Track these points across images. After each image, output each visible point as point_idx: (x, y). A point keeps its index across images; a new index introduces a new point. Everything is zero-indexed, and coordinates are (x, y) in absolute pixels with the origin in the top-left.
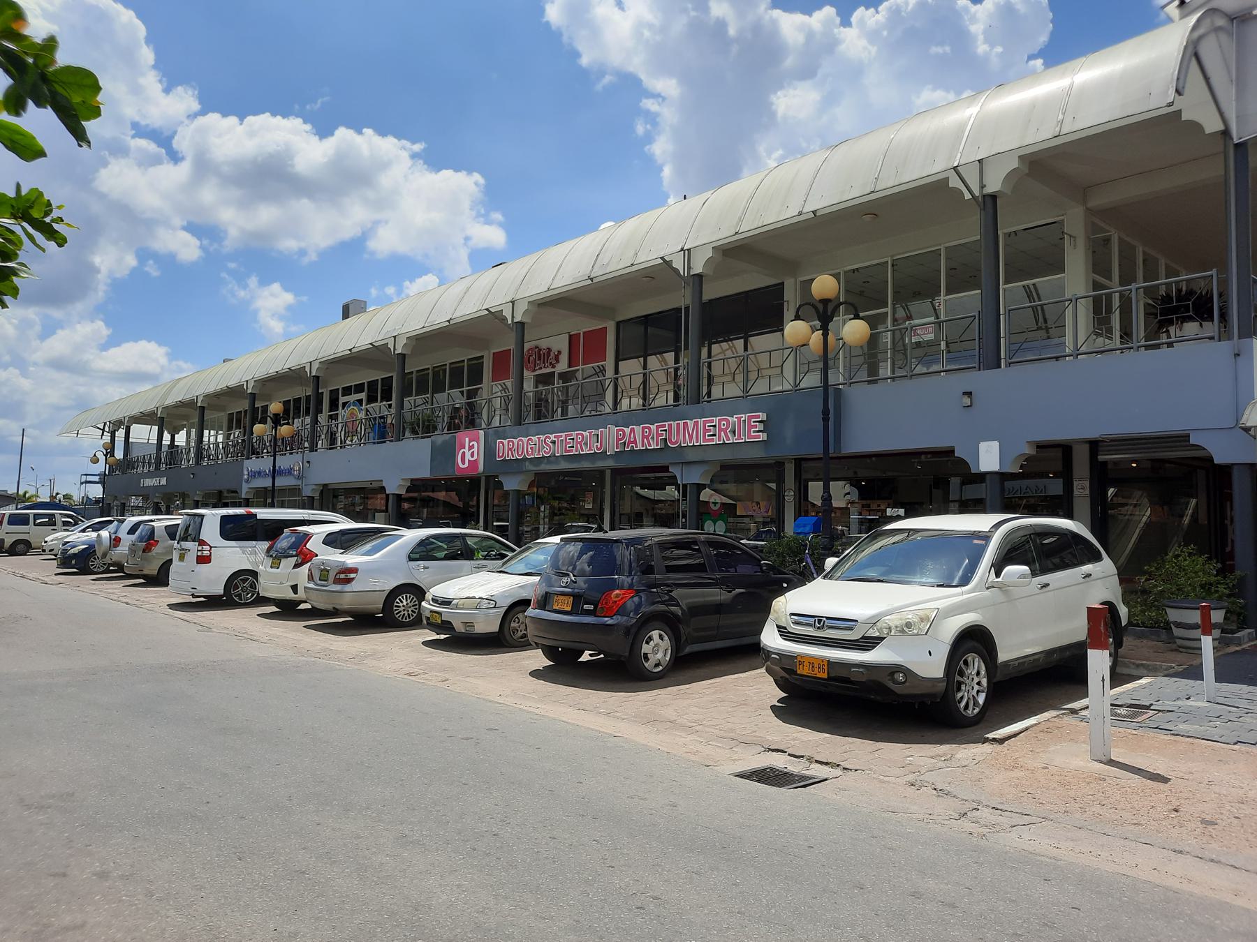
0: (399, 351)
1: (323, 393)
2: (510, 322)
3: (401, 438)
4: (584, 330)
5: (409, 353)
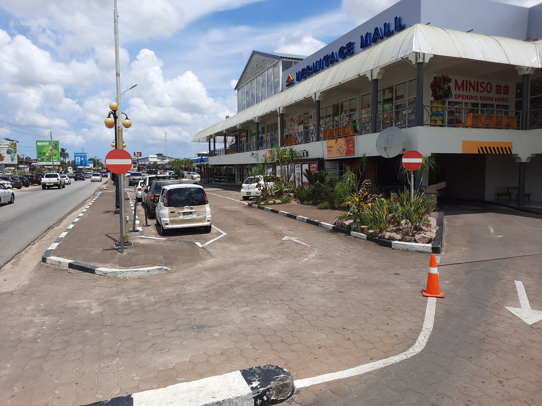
0: (317, 99)
1: (286, 120)
2: (370, 79)
3: (377, 130)
4: (340, 102)
5: (322, 100)
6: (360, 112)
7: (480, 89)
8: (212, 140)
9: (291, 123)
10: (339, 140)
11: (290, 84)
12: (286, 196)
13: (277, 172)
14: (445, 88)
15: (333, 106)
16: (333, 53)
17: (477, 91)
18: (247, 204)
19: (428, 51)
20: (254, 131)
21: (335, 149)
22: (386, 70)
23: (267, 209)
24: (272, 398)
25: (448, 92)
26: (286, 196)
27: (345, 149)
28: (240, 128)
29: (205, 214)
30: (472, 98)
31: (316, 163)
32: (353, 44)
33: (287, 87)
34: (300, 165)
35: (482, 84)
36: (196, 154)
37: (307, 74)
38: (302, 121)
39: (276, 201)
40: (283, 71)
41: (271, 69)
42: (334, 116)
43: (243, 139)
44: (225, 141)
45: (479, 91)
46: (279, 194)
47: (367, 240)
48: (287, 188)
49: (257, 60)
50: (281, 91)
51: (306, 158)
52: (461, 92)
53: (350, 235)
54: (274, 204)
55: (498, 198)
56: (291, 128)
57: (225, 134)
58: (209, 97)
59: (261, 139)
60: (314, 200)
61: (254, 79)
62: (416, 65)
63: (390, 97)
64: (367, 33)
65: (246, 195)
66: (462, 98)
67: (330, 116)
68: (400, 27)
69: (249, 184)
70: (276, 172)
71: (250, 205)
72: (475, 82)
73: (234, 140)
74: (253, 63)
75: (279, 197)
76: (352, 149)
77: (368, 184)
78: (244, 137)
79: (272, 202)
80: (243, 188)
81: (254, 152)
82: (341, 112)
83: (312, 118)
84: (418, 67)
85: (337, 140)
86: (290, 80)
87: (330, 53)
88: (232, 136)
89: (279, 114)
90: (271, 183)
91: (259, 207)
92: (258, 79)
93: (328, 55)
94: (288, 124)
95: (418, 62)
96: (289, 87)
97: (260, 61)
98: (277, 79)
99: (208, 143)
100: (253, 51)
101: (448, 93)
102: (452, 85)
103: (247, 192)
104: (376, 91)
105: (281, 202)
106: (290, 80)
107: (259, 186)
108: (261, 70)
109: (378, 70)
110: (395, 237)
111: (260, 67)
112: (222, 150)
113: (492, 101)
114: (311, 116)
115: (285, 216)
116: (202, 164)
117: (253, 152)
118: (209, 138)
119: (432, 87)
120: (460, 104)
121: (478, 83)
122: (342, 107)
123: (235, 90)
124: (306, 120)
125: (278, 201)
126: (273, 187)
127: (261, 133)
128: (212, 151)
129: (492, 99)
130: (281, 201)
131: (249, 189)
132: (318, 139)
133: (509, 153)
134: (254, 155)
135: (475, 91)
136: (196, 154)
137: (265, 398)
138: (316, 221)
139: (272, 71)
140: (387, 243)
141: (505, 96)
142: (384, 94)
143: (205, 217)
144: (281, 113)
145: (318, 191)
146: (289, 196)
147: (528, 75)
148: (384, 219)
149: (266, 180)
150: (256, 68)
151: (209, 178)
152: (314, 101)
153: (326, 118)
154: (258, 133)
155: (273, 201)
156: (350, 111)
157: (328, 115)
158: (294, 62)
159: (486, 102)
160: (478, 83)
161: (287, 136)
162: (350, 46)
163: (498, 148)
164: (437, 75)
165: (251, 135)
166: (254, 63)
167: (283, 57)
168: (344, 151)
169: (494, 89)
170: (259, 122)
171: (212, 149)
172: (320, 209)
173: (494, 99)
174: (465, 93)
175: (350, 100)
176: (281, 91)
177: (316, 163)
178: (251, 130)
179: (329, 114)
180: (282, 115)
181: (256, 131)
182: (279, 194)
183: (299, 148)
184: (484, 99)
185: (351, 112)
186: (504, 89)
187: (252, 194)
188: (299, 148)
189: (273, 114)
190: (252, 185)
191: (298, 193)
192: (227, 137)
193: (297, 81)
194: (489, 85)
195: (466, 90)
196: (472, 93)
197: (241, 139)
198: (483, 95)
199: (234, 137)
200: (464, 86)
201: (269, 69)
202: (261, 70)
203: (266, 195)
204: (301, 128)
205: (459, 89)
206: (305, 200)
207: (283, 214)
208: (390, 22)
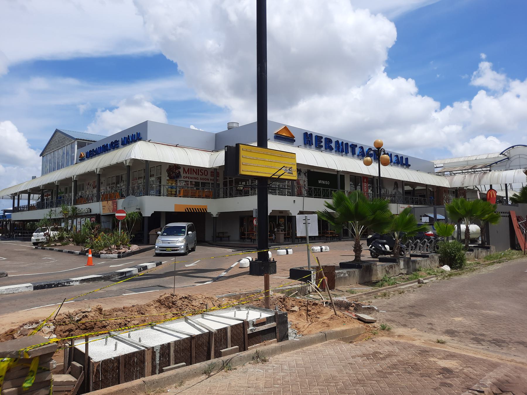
0: (127, 164)
7: (200, 173)
8: (16, 197)
9: (88, 187)
10: (109, 202)
13: (69, 225)
15: (144, 170)
17: (198, 175)
18: (34, 247)
21: (106, 208)
30: (195, 178)
34: (84, 219)
36: (1, 210)
40: (78, 148)
41: (69, 145)
43: (49, 197)
45: (199, 174)
50: (76, 164)
51: (90, 214)
52: (187, 175)
53: (86, 255)
58: (30, 149)
64: (124, 137)
65: (35, 241)
66: (188, 179)
69: (38, 233)
71: (36, 248)
72: (196, 169)
76: (116, 208)
78: (49, 195)
79: (54, 244)
80: (33, 236)
81: (52, 209)
85: (108, 202)
88: (39, 194)
92: (59, 151)
100: (56, 129)
105: (61, 244)
109: (129, 161)
112: (25, 206)
114: (102, 182)
116: (4, 220)
122: (122, 177)
123: (40, 156)
127: (64, 193)
128: (16, 207)
131: (38, 236)
132: (98, 201)
133: (205, 212)
136: (1, 210)
144: (74, 179)
151: (10, 233)
158: (88, 143)
159: (204, 181)
163: (203, 209)
166: (56, 138)
170: (131, 165)
171: (16, 205)
173: (210, 180)
174: (190, 175)
176: (76, 164)
179: (113, 182)
180: (76, 181)
182: (61, 239)
188: (83, 207)
194: (206, 172)
195: (191, 174)
196: (194, 175)
198: (202, 177)
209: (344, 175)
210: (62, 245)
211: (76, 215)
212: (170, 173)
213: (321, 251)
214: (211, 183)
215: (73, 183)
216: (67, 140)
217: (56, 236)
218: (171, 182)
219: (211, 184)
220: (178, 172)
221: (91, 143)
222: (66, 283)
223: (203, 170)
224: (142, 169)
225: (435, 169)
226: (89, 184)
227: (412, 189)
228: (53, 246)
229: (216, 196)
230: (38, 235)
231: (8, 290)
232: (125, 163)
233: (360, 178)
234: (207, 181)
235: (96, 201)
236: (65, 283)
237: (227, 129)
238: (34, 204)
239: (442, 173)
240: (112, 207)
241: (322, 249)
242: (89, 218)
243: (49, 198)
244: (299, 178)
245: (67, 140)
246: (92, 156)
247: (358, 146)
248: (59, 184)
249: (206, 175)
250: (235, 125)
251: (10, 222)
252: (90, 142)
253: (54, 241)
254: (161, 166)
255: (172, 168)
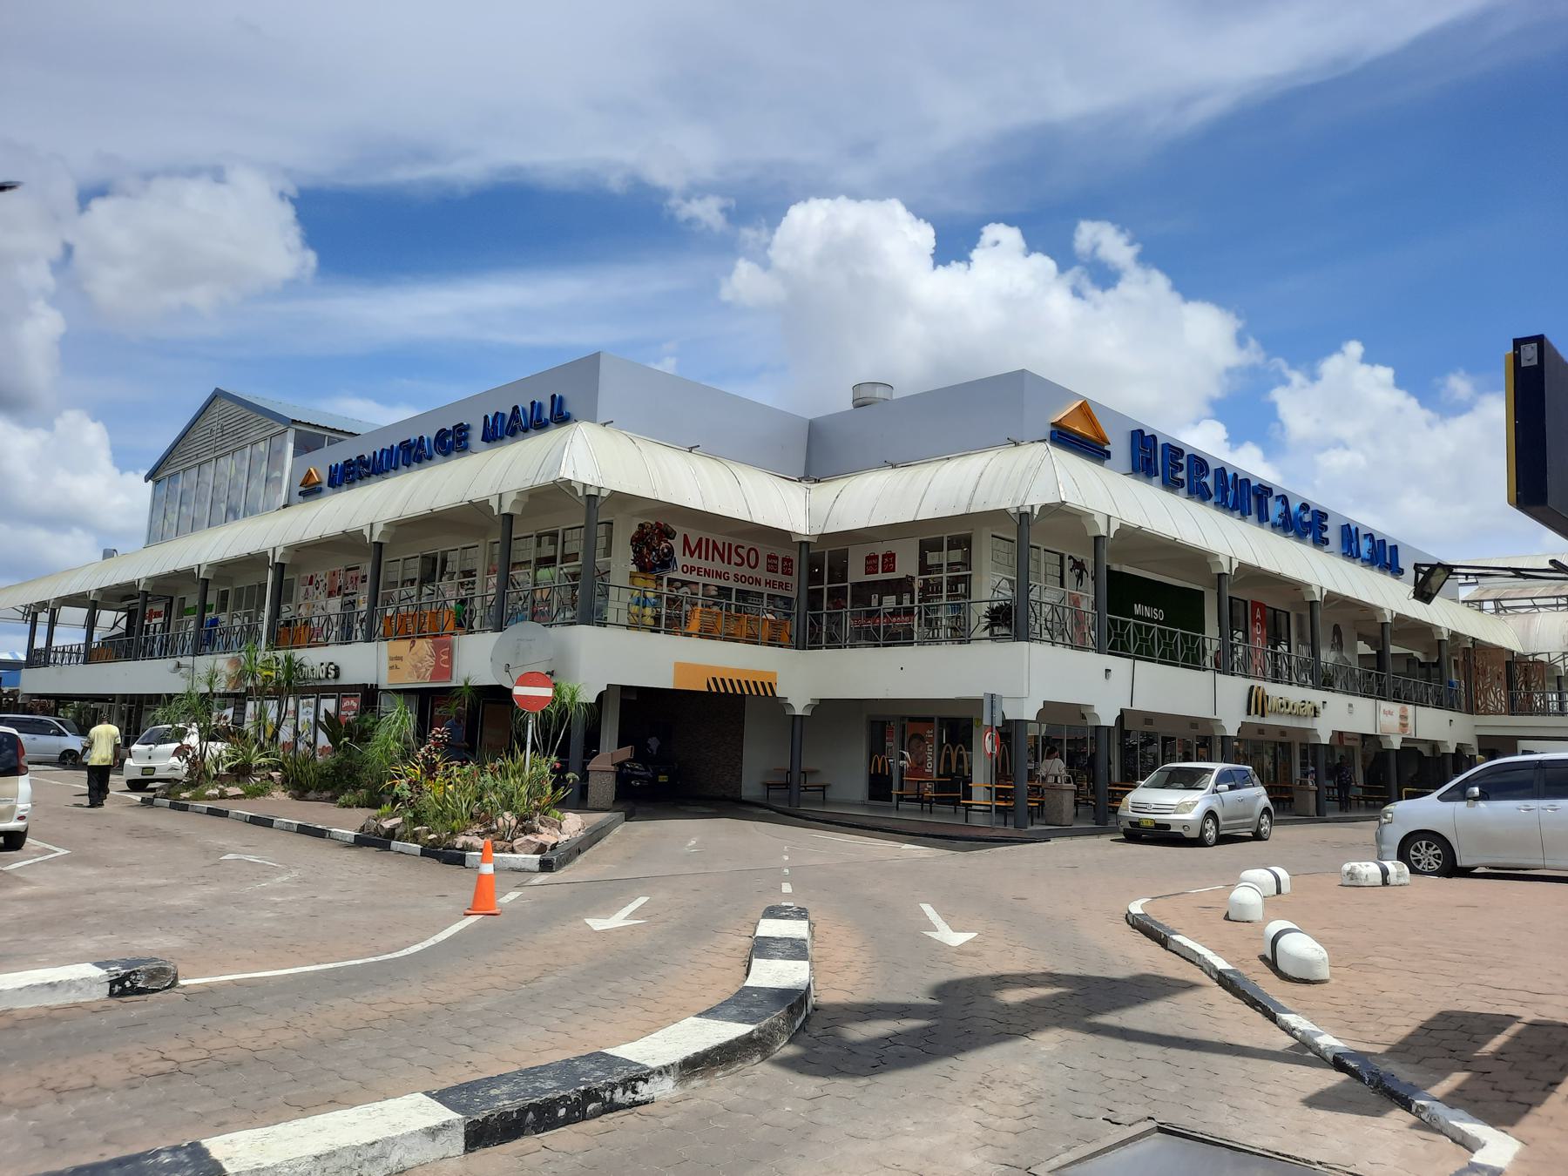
0: (375, 539)
5: (388, 542)
6: (485, 580)
7: (744, 552)
8: (44, 617)
10: (418, 642)
11: (310, 490)
12: (259, 779)
13: (246, 719)
14: (663, 550)
15: (537, 537)
16: (421, 438)
17: (729, 563)
18: (139, 799)
19: (593, 479)
20: (193, 601)
22: (530, 496)
23: (198, 809)
24: (139, 985)
25: (667, 559)
26: (259, 779)
27: (431, 666)
28: (149, 589)
29: (15, 801)
30: (719, 575)
31: (356, 696)
32: (468, 427)
33: (302, 497)
34: (312, 700)
35: (739, 550)
37: (356, 475)
38: (340, 588)
39: (227, 789)
40: (295, 455)
42: (422, 583)
44: (91, 623)
45: (733, 563)
46: (240, 772)
47: (421, 855)
48: (267, 756)
49: (225, 415)
50: (285, 506)
51: (332, 682)
52: (694, 561)
54: (220, 798)
55: (768, 793)
56: (307, 601)
57: (92, 603)
59: (211, 626)
60: (336, 789)
61: (211, 460)
62: (584, 498)
63: (552, 554)
64: (497, 413)
65: (140, 777)
66: (698, 574)
67: (412, 582)
68: (561, 417)
69: (152, 746)
70: (244, 719)
72: (724, 544)
73: (123, 624)
74: (214, 420)
75: (238, 781)
76: (447, 666)
77: (440, 736)
78: (158, 615)
79: (216, 792)
80: (131, 757)
81: (183, 661)
82: (442, 575)
83: (365, 581)
84: (588, 503)
86: (312, 481)
87: (414, 437)
88: (118, 610)
89: (270, 564)
90: (219, 744)
91: (173, 806)
93: (409, 440)
94: (300, 591)
95: (587, 494)
96: (309, 498)
97: (234, 420)
98: (277, 474)
99: (28, 626)
101: (667, 561)
102: (677, 544)
103: (144, 768)
104: (508, 542)
105: (242, 792)
106: (312, 481)
107: (181, 752)
108: (233, 442)
109: (514, 497)
110: (476, 844)
111: (231, 434)
113: (760, 585)
114: (365, 577)
115: (246, 821)
117: (179, 659)
118: (31, 614)
119: (634, 543)
120: (693, 587)
121: (730, 545)
122: (444, 562)
123: (146, 481)
124: (350, 586)
125: (234, 790)
126: (224, 752)
128: (37, 650)
129: (758, 582)
130: (243, 790)
131: (150, 758)
134: (183, 670)
135: (724, 562)
137: (128, 984)
138: (320, 827)
139: (265, 449)
140: (456, 858)
141: (785, 579)
142: (539, 544)
143: (12, 809)
144: (277, 560)
145: (351, 765)
146: (269, 778)
147: (808, 543)
148: (464, 810)
149: (209, 735)
150: (221, 434)
152: (496, 513)
153: (402, 586)
154: (205, 608)
155: (220, 789)
156: (461, 575)
157: (408, 580)
158: (329, 437)
159: (746, 587)
160: (730, 545)
161: (288, 623)
162: (460, 431)
164: (646, 521)
165: (183, 612)
167: (300, 421)
168: (427, 670)
169: (763, 562)
170: (210, 577)
172: (344, 807)
173: (763, 582)
174: (703, 564)
175: (464, 548)
176: (285, 506)
177: (356, 696)
178: (184, 598)
180: (280, 568)
181: (197, 604)
182: (240, 772)
183: (313, 658)
184: (743, 580)
185: (465, 577)
186: (783, 563)
187: (157, 775)
188: (313, 658)
189: (255, 561)
190: (161, 747)
191: (296, 771)
192: (97, 611)
193: (329, 486)
194: (752, 553)
195: (707, 559)
196: (717, 565)
197: (146, 622)
199: (124, 614)
200: (694, 549)
201: (256, 443)
202: (233, 442)
203: (200, 773)
204: (335, 604)
205: (692, 555)
206: (311, 789)
207: (239, 818)
208: (541, 401)
209: (1203, 592)
210: (247, 794)
211: (293, 685)
212: (641, 550)
213: (1385, 883)
214: (768, 595)
215: (270, 573)
216: (255, 424)
217: (223, 765)
218: (640, 582)
219: (765, 596)
220: (666, 550)
221: (340, 440)
222: (620, 1090)
223: (743, 547)
224: (530, 534)
225: (1460, 588)
226: (315, 582)
227: (1374, 652)
228: (214, 798)
229: (810, 639)
230: (150, 754)
231: (329, 1164)
232: (367, 533)
233: (1242, 604)
234: (754, 588)
235: (359, 639)
236: (613, 1087)
237: (847, 405)
238: (64, 646)
239: (1478, 603)
240: (430, 661)
241: (1385, 872)
242: (275, 699)
243: (155, 625)
244: (1080, 591)
245: (255, 424)
246: (352, 482)
247: (1276, 493)
248: (212, 575)
249: (753, 564)
250: (880, 393)
251: (16, 700)
252: (340, 435)
253: (214, 779)
254: (611, 523)
255: (647, 534)
